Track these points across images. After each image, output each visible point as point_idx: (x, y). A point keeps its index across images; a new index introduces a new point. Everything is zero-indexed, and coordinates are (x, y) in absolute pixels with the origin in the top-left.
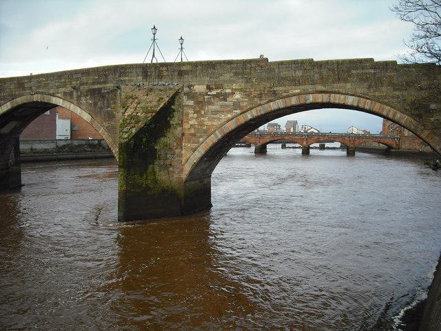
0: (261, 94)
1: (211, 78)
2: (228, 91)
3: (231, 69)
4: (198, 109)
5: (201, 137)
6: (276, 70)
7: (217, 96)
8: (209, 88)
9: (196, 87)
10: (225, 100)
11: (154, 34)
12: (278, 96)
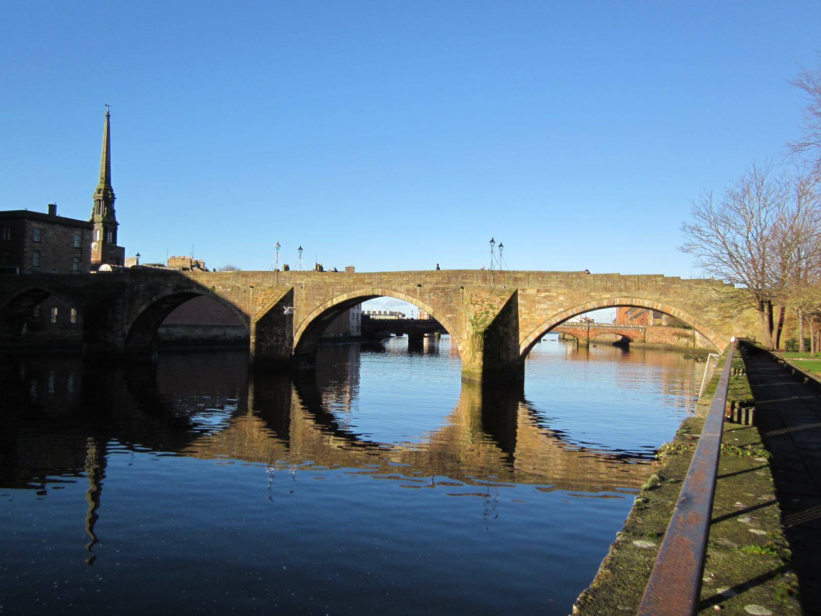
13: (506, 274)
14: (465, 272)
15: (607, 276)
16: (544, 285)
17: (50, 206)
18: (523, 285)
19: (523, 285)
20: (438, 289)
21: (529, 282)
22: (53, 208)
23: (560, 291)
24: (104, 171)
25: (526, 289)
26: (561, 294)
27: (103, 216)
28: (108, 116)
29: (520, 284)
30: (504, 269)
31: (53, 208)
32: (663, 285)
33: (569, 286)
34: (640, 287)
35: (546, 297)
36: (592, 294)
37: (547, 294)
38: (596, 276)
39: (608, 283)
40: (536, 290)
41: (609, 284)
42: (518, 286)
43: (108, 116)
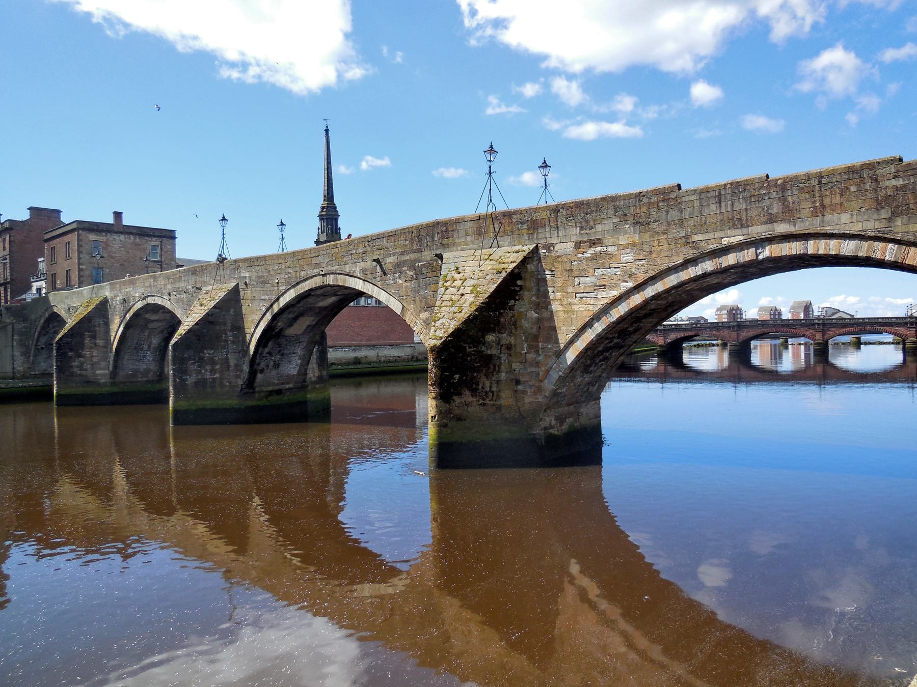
13: (514, 216)
14: (445, 223)
15: (737, 188)
16: (588, 231)
17: (115, 213)
18: (548, 236)
19: (548, 236)
20: (404, 263)
21: (558, 228)
22: (118, 215)
23: (623, 240)
24: (326, 188)
25: (553, 245)
26: (626, 247)
27: (327, 235)
28: (327, 130)
29: (541, 236)
30: (513, 207)
31: (118, 215)
32: (896, 188)
33: (640, 224)
34: (827, 201)
35: (594, 258)
36: (697, 238)
37: (598, 249)
38: (703, 193)
39: (736, 204)
40: (572, 245)
41: (740, 205)
42: (537, 239)
43: (327, 130)
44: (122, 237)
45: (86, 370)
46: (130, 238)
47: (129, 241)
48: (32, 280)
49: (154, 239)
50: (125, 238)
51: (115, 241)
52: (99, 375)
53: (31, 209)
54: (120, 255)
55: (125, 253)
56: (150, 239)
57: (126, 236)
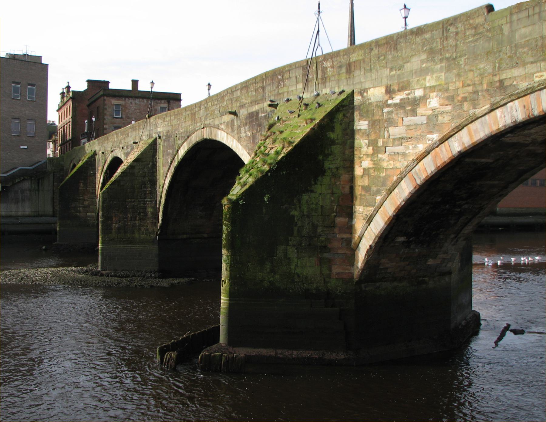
0: (476, 92)
1: (391, 69)
2: (419, 93)
3: (424, 45)
4: (373, 137)
5: (378, 192)
6: (506, 29)
7: (401, 106)
8: (390, 92)
9: (371, 92)
10: (414, 113)
11: (209, 90)
12: (509, 91)
22: (135, 83)
31: (135, 83)
40: (383, 90)
44: (137, 101)
45: (80, 212)
46: (144, 102)
47: (142, 103)
48: (81, 138)
49: (163, 101)
50: (140, 101)
51: (132, 104)
52: (89, 216)
53: (89, 82)
54: (135, 116)
55: (138, 114)
56: (160, 102)
57: (141, 100)
